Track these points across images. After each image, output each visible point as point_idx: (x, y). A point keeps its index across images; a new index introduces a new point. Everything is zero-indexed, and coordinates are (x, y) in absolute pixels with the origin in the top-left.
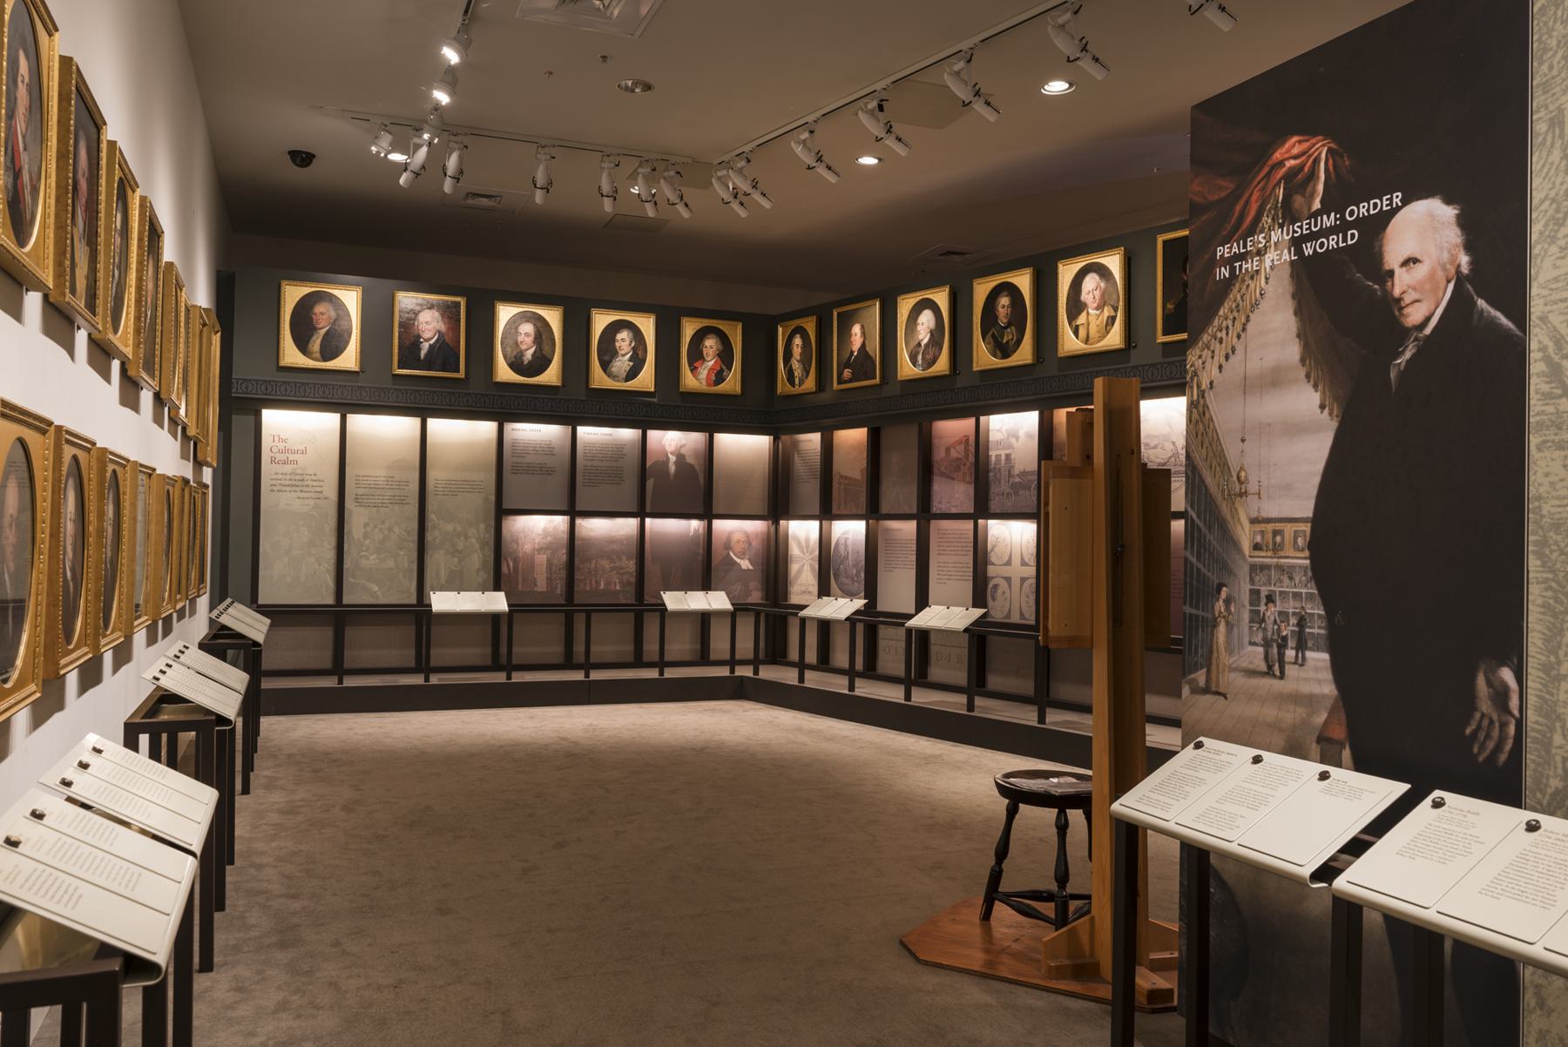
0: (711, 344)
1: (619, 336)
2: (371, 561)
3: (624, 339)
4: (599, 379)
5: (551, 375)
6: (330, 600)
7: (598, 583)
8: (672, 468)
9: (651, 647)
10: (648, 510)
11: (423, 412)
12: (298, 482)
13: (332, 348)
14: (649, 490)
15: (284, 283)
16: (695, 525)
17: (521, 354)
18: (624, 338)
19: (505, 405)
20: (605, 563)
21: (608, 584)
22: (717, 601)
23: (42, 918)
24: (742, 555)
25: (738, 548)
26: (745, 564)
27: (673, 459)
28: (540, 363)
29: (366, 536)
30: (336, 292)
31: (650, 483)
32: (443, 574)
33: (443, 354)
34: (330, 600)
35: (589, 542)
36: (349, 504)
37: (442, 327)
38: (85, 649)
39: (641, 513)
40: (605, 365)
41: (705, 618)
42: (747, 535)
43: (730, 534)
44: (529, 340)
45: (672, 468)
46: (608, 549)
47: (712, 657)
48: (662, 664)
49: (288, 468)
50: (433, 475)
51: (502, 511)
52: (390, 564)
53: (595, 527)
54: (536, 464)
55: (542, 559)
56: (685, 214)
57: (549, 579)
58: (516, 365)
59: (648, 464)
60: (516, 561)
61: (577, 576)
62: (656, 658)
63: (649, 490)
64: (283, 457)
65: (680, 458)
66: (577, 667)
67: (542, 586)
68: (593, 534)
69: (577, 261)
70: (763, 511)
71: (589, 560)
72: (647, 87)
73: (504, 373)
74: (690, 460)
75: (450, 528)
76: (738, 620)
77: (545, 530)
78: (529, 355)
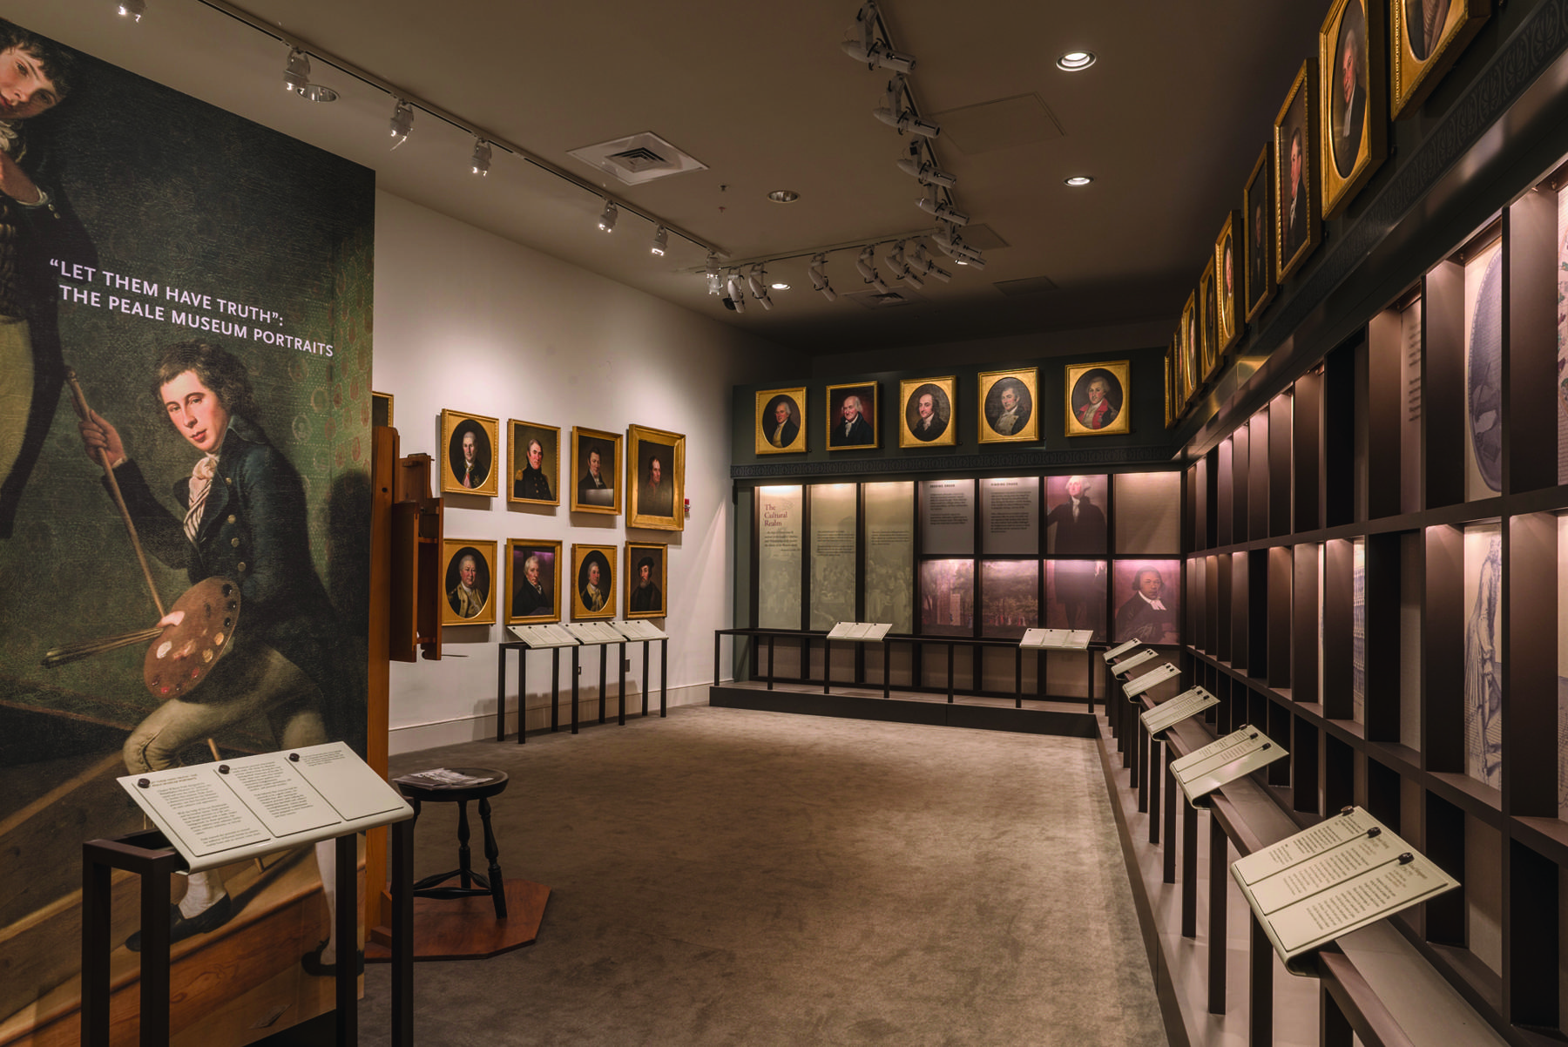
0: (1096, 386)
1: (1005, 394)
2: (828, 598)
3: (1009, 396)
4: (989, 435)
5: (946, 437)
6: (797, 626)
7: (1006, 620)
8: (1076, 511)
9: (817, 672)
10: (1052, 551)
11: (859, 478)
12: (782, 538)
13: (789, 437)
14: (1055, 532)
15: (980, 375)
16: (1100, 565)
17: (922, 422)
18: (783, 408)
19: (922, 467)
20: (1012, 602)
21: (1014, 621)
22: (874, 631)
23: (1389, 918)
24: (1153, 596)
25: (1148, 588)
26: (1157, 605)
27: (1076, 502)
28: (938, 428)
29: (825, 578)
30: (937, 383)
31: (1053, 529)
32: (879, 610)
33: (862, 431)
34: (797, 626)
35: (996, 582)
36: (814, 553)
37: (860, 408)
38: (1117, 669)
39: (1042, 555)
40: (993, 422)
41: (861, 646)
42: (1158, 575)
43: (1139, 574)
44: (928, 409)
45: (1076, 511)
46: (1013, 587)
47: (812, 677)
48: (827, 683)
49: (776, 528)
50: (872, 529)
51: (921, 554)
52: (842, 600)
53: (1001, 569)
54: (1010, 508)
55: (956, 598)
56: (917, 286)
57: (963, 616)
58: (918, 432)
59: (1049, 510)
60: (934, 598)
61: (985, 612)
62: (1086, 695)
63: (1055, 532)
64: (771, 520)
65: (1084, 499)
66: (762, 679)
67: (956, 621)
68: (1000, 575)
69: (960, 335)
70: (1175, 551)
71: (997, 599)
72: (795, 196)
73: (909, 439)
74: (1094, 502)
75: (883, 571)
76: (893, 655)
77: (959, 572)
78: (928, 421)
